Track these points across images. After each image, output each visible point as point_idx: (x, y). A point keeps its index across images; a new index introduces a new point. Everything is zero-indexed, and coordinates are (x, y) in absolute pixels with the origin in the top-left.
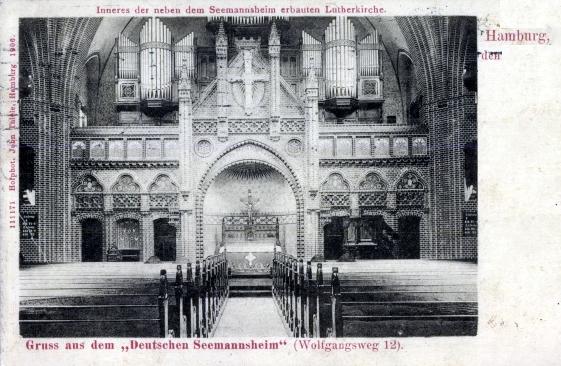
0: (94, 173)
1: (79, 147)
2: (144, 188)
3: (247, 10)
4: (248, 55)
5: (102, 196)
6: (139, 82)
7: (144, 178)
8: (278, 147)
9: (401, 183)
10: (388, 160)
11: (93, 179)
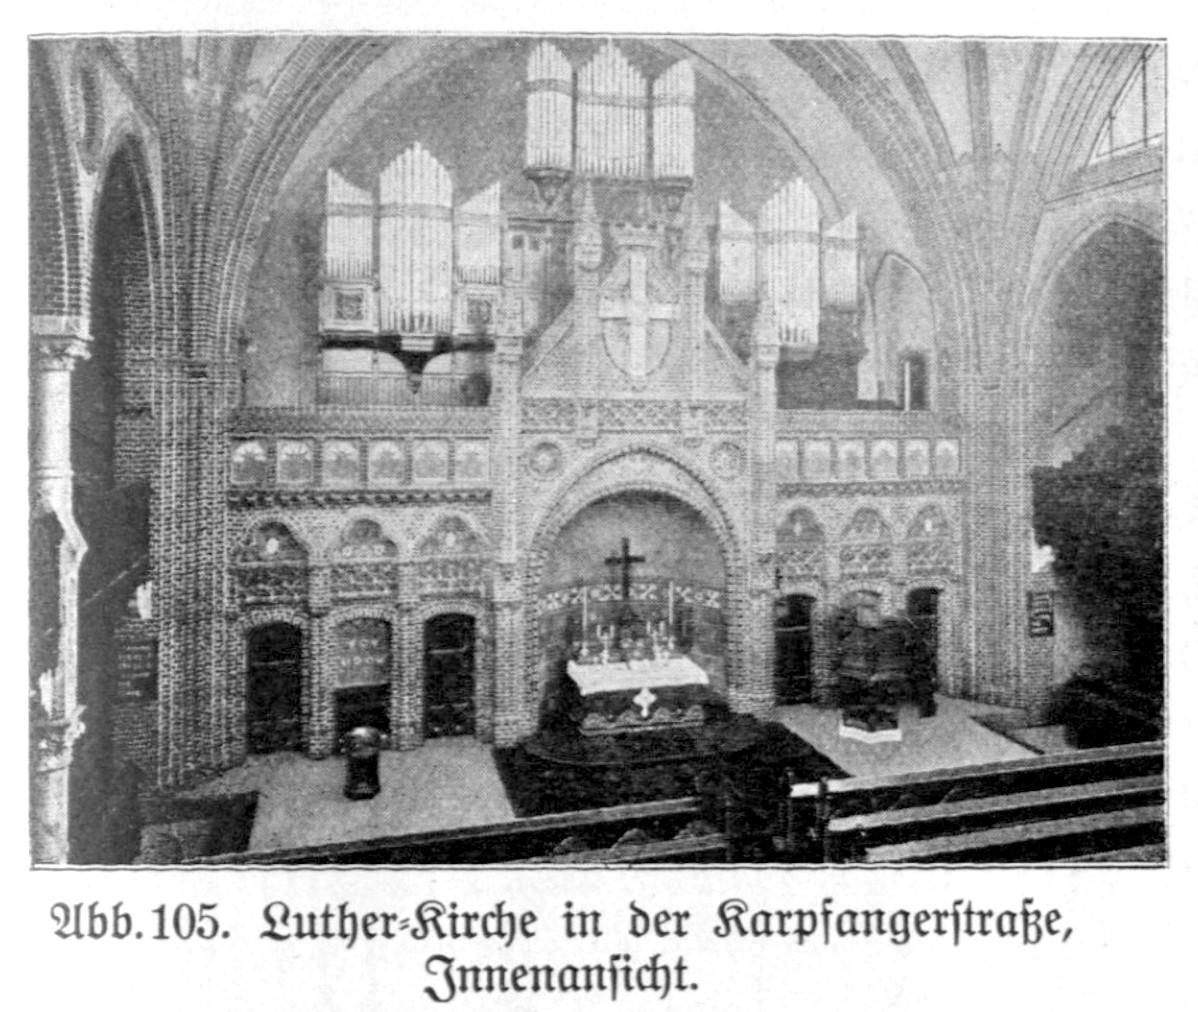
0: (285, 517)
1: (250, 458)
2: (408, 549)
3: (965, 920)
4: (639, 261)
5: (307, 572)
6: (377, 289)
7: (405, 527)
8: (701, 462)
9: (917, 527)
10: (896, 485)
11: (283, 530)
